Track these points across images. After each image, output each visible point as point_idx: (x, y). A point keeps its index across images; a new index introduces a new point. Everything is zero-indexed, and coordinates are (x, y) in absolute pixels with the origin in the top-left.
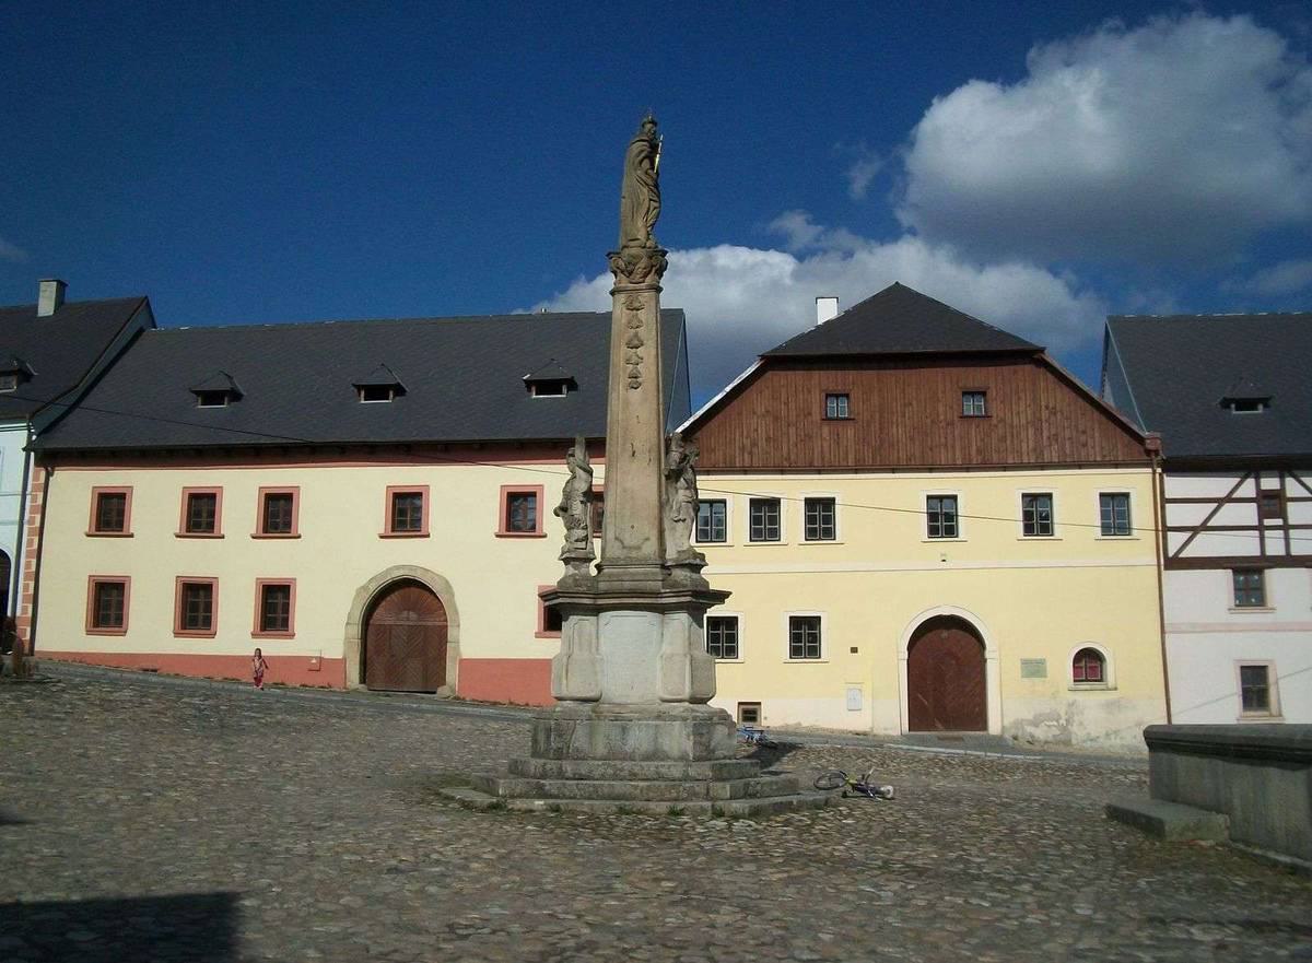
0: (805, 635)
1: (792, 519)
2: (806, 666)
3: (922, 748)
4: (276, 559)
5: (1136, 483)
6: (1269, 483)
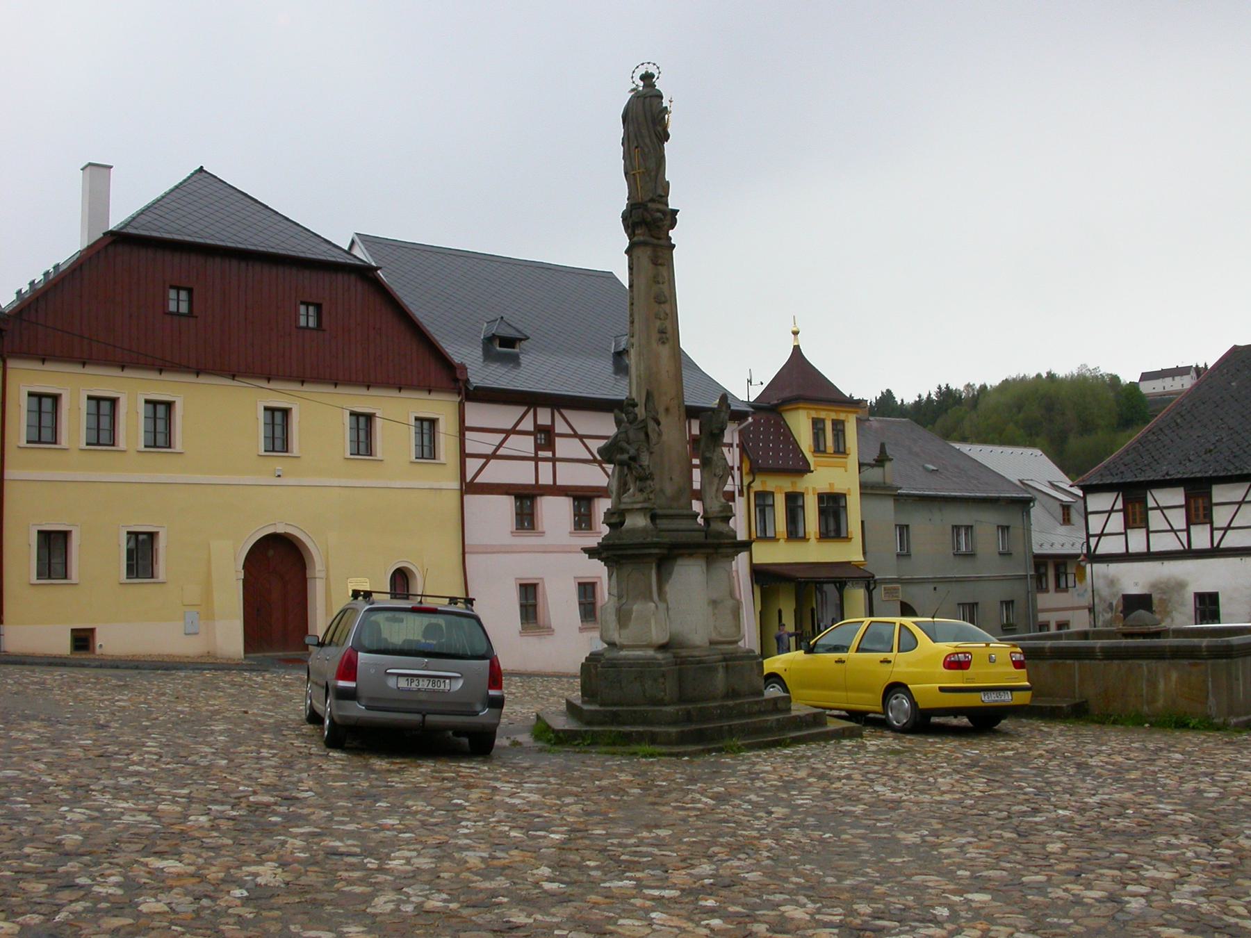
0: (141, 554)
1: (132, 423)
2: (142, 590)
3: (615, 709)
5: (441, 407)
6: (544, 417)
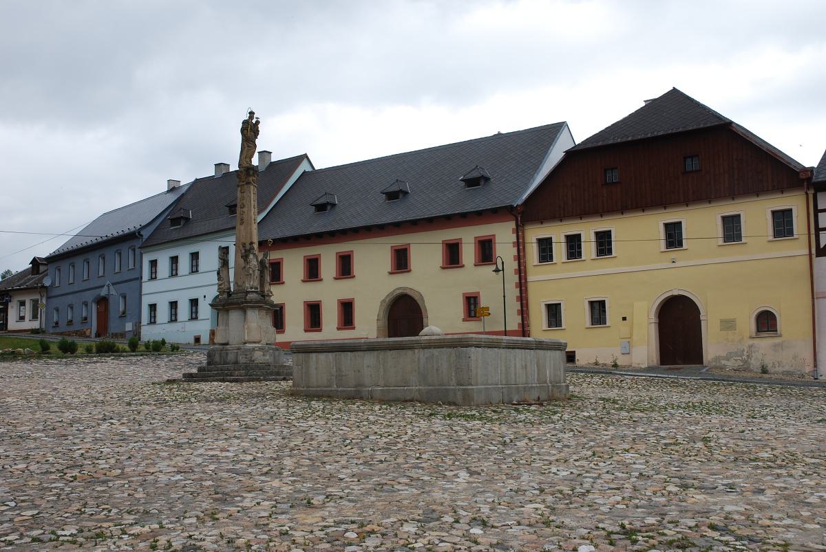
0: (598, 311)
4: (345, 289)
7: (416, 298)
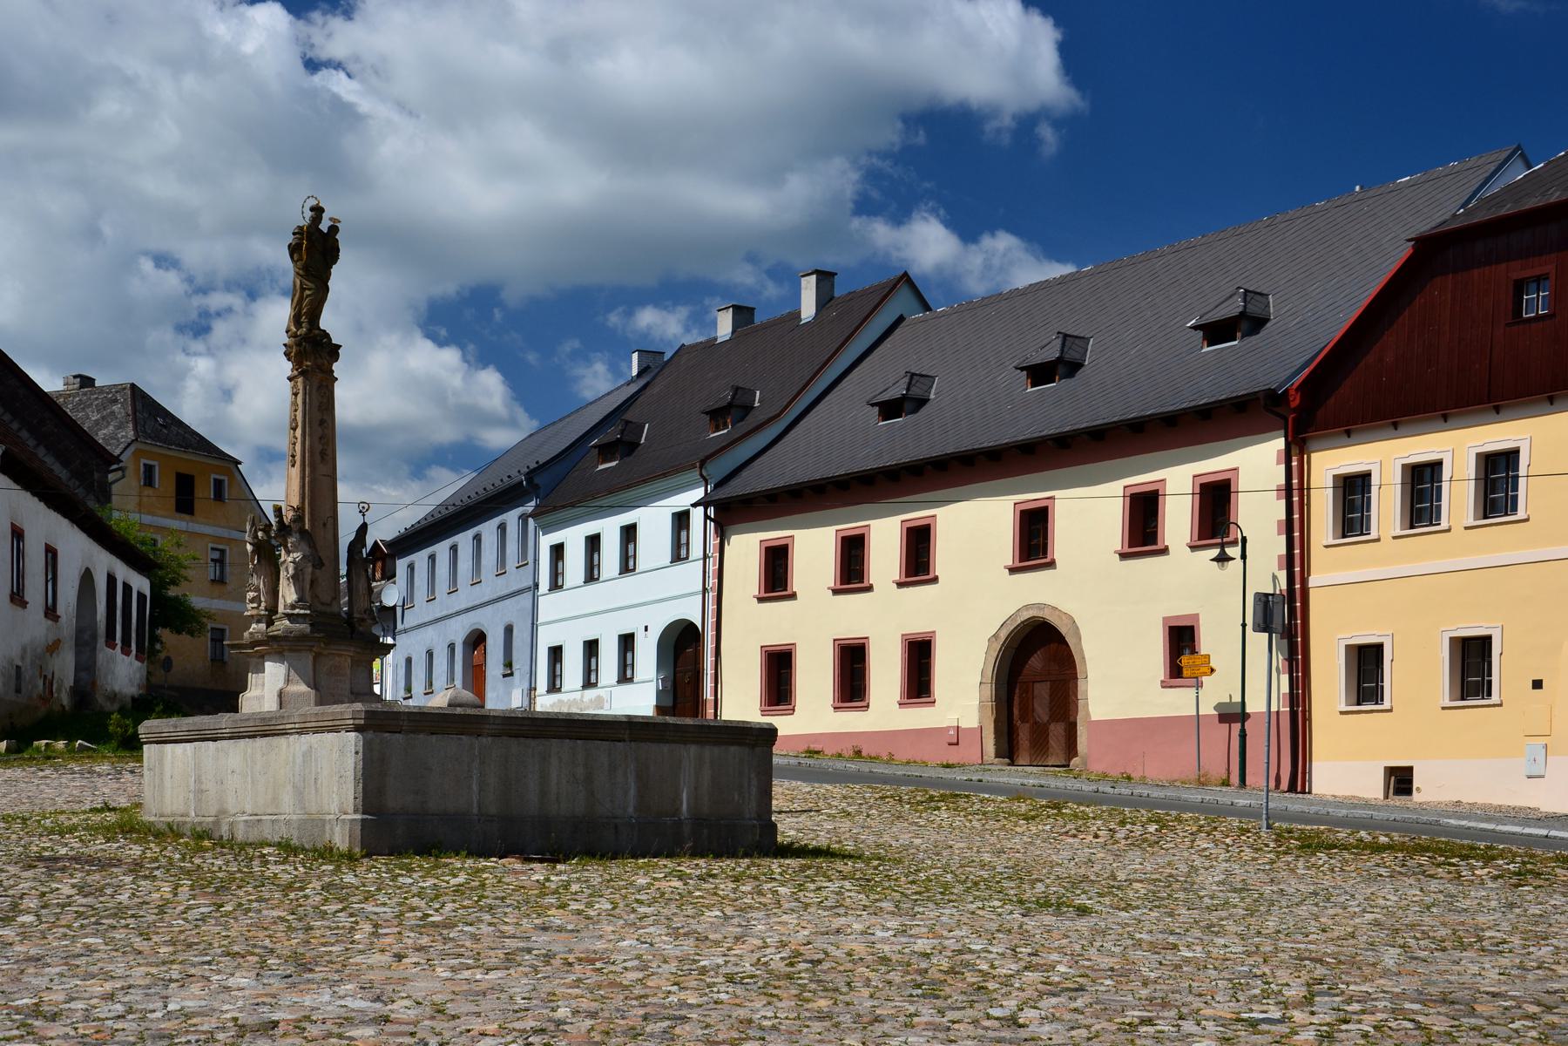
7: (1063, 631)
